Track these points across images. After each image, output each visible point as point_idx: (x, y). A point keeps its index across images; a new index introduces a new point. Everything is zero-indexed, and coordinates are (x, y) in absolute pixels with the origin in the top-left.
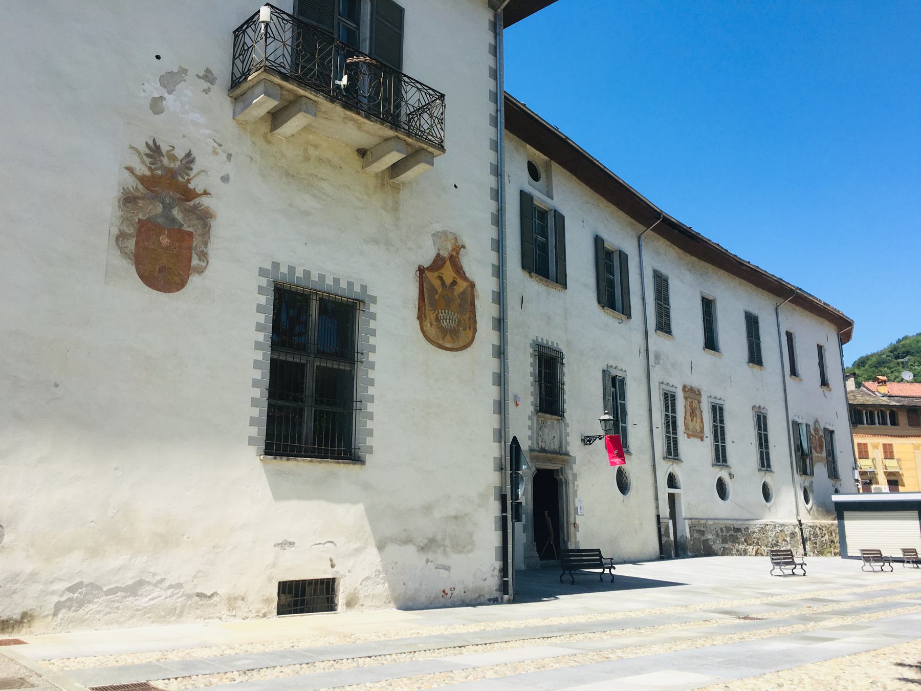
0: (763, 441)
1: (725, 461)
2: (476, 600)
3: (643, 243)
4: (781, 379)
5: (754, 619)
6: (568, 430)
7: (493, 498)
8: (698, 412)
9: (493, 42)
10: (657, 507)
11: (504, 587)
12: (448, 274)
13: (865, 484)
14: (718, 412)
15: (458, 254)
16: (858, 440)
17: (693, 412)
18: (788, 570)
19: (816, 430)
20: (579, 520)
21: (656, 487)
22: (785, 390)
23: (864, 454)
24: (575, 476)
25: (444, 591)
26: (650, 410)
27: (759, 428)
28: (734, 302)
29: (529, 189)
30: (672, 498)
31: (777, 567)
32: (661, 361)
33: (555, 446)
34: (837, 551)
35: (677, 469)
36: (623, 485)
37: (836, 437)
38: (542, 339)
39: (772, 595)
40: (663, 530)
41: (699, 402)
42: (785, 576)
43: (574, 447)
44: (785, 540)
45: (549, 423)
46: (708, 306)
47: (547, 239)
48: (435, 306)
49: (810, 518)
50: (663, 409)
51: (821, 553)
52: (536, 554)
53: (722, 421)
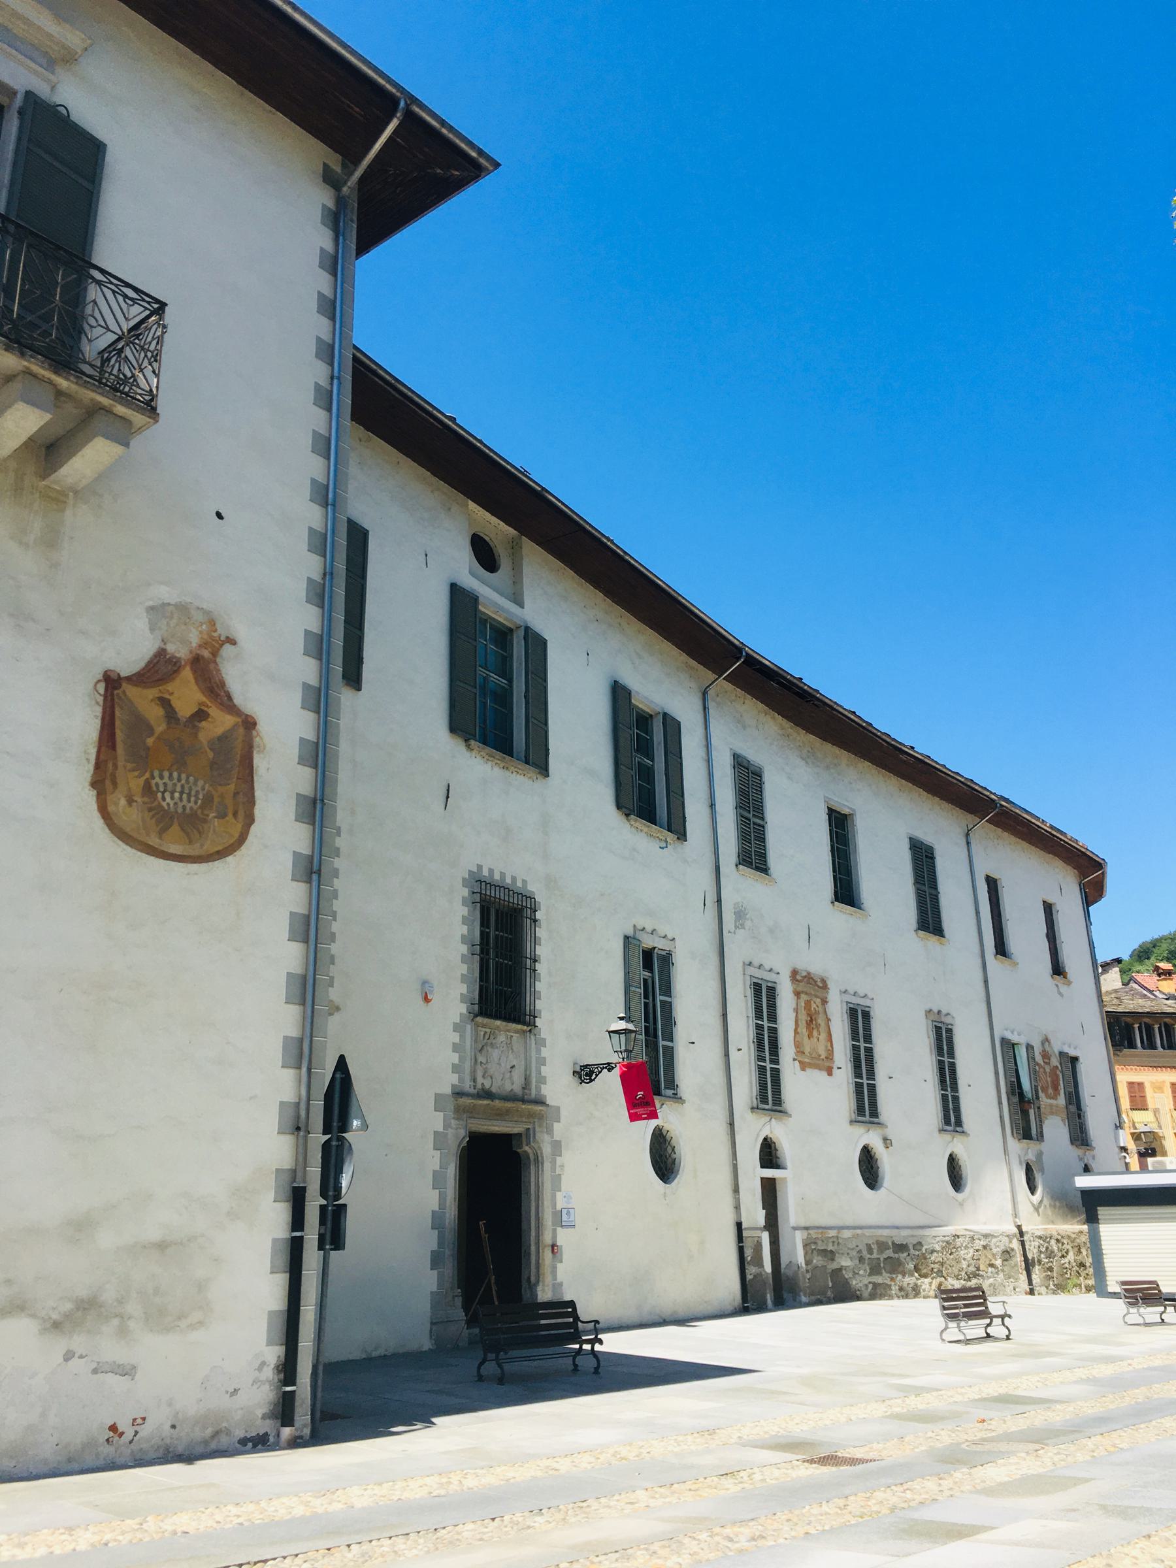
0: (947, 1076)
1: (874, 1113)
2: (206, 1442)
3: (711, 705)
4: (979, 961)
5: (853, 1462)
6: (544, 1052)
7: (271, 1195)
8: (821, 1020)
9: (329, 246)
10: (737, 1207)
11: (284, 1410)
12: (186, 695)
13: (1144, 1155)
14: (860, 1020)
15: (215, 653)
16: (1125, 1076)
17: (812, 1020)
18: (975, 1328)
19: (1046, 1056)
20: (563, 1237)
21: (735, 1168)
22: (986, 982)
23: (1138, 1102)
24: (557, 1147)
25: (113, 1428)
26: (724, 1015)
27: (940, 1051)
28: (889, 821)
29: (470, 582)
30: (770, 1190)
31: (952, 1325)
32: (748, 924)
33: (514, 1084)
34: (1091, 1282)
35: (777, 1130)
36: (664, 1163)
37: (1083, 1068)
38: (491, 871)
39: (918, 1391)
40: (748, 1253)
41: (824, 1002)
42: (968, 1342)
43: (557, 1087)
44: (992, 1265)
45: (502, 1038)
46: (840, 826)
47: (510, 681)
48: (142, 759)
49: (1041, 1222)
50: (751, 1013)
51: (1060, 1288)
52: (461, 1314)
53: (868, 1038)
